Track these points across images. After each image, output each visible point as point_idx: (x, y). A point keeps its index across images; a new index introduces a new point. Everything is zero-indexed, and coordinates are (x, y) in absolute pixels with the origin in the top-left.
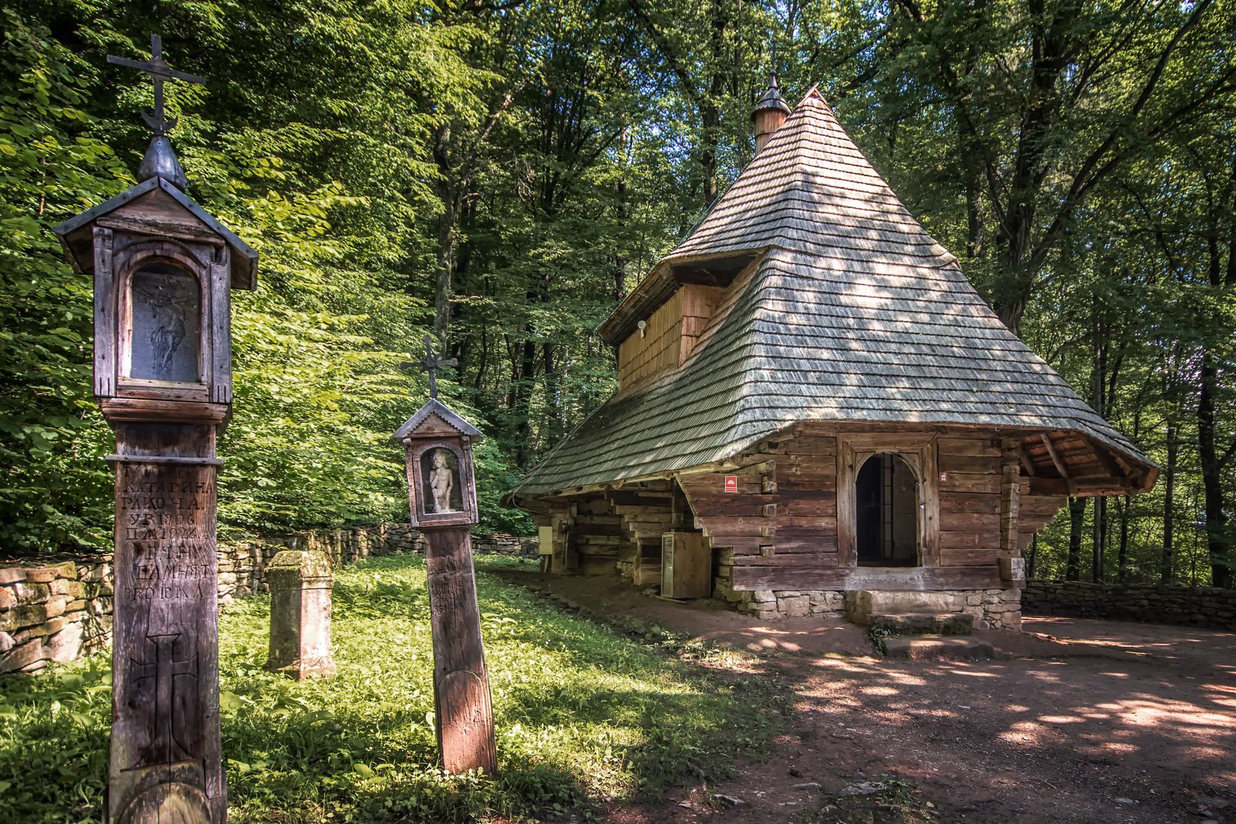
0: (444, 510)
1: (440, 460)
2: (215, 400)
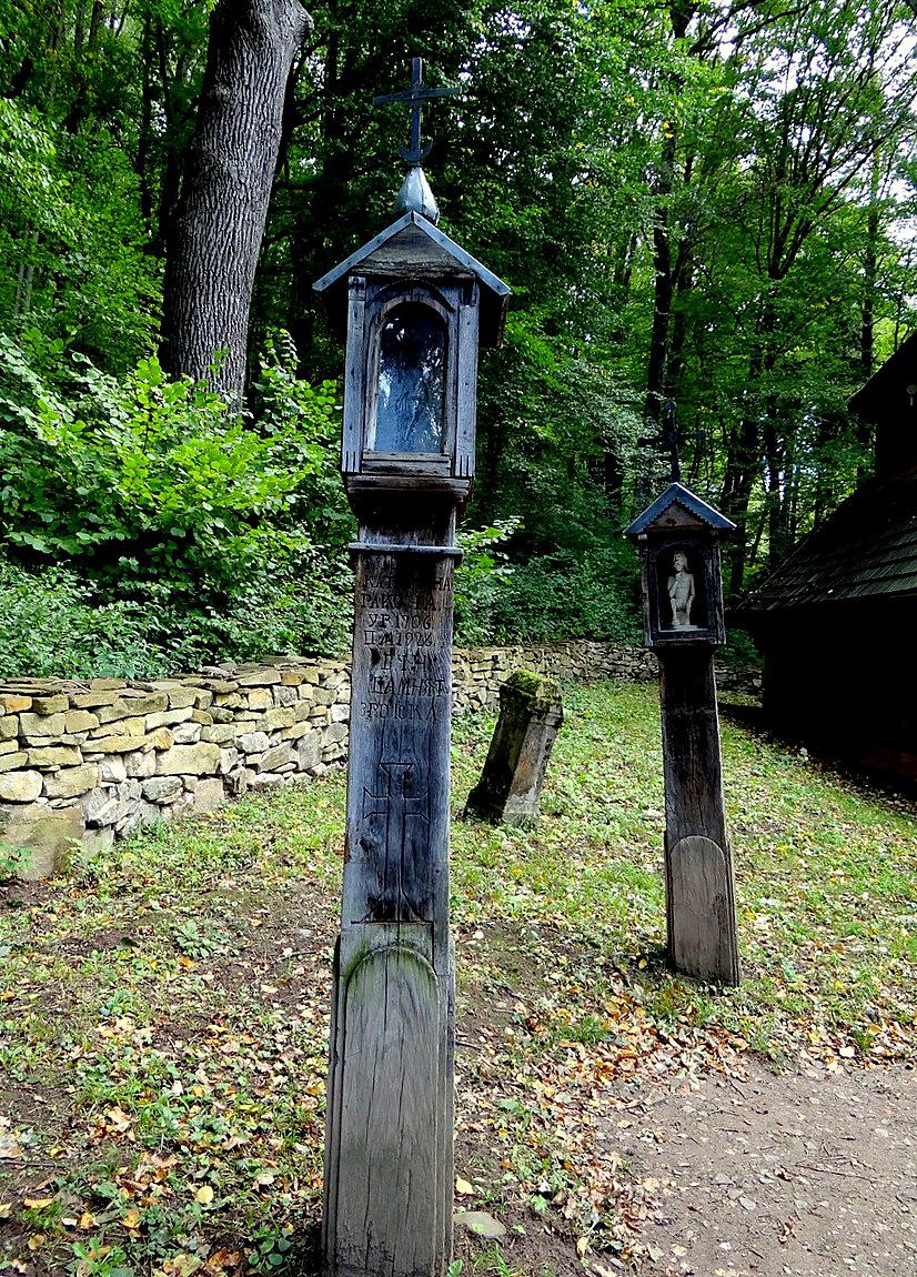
0: (682, 625)
1: (680, 561)
2: (458, 474)
